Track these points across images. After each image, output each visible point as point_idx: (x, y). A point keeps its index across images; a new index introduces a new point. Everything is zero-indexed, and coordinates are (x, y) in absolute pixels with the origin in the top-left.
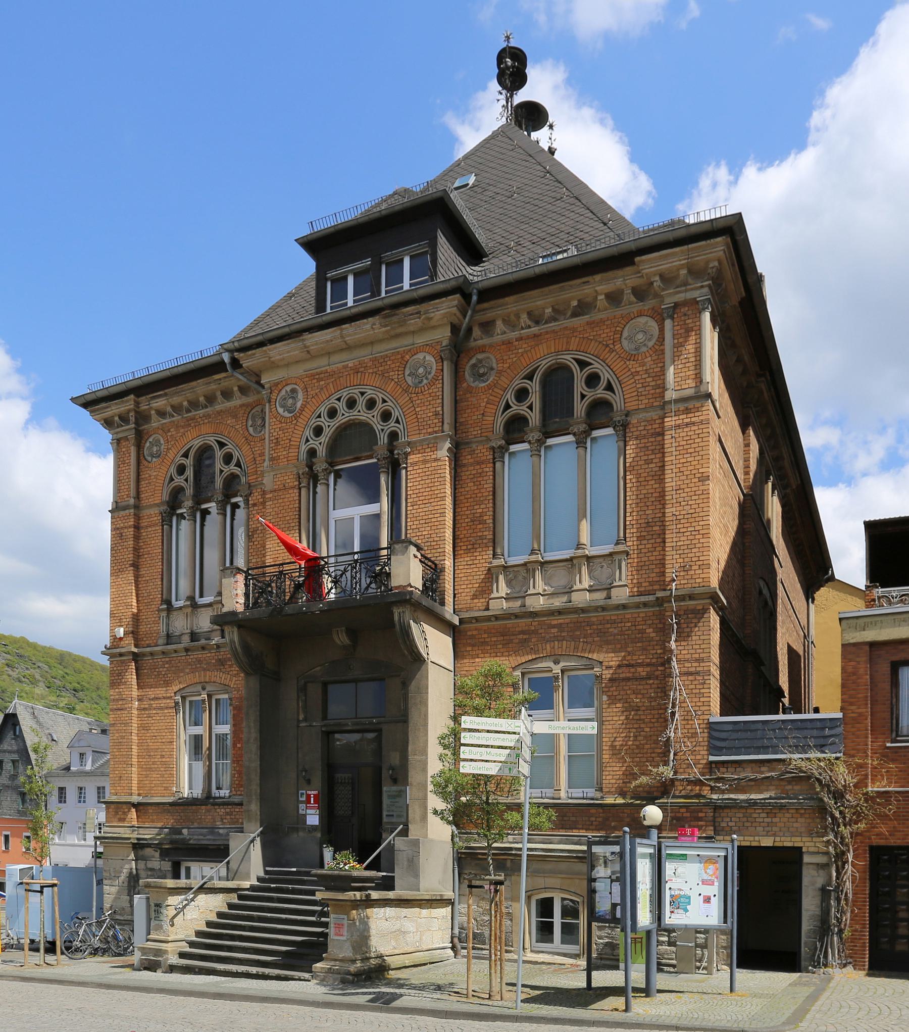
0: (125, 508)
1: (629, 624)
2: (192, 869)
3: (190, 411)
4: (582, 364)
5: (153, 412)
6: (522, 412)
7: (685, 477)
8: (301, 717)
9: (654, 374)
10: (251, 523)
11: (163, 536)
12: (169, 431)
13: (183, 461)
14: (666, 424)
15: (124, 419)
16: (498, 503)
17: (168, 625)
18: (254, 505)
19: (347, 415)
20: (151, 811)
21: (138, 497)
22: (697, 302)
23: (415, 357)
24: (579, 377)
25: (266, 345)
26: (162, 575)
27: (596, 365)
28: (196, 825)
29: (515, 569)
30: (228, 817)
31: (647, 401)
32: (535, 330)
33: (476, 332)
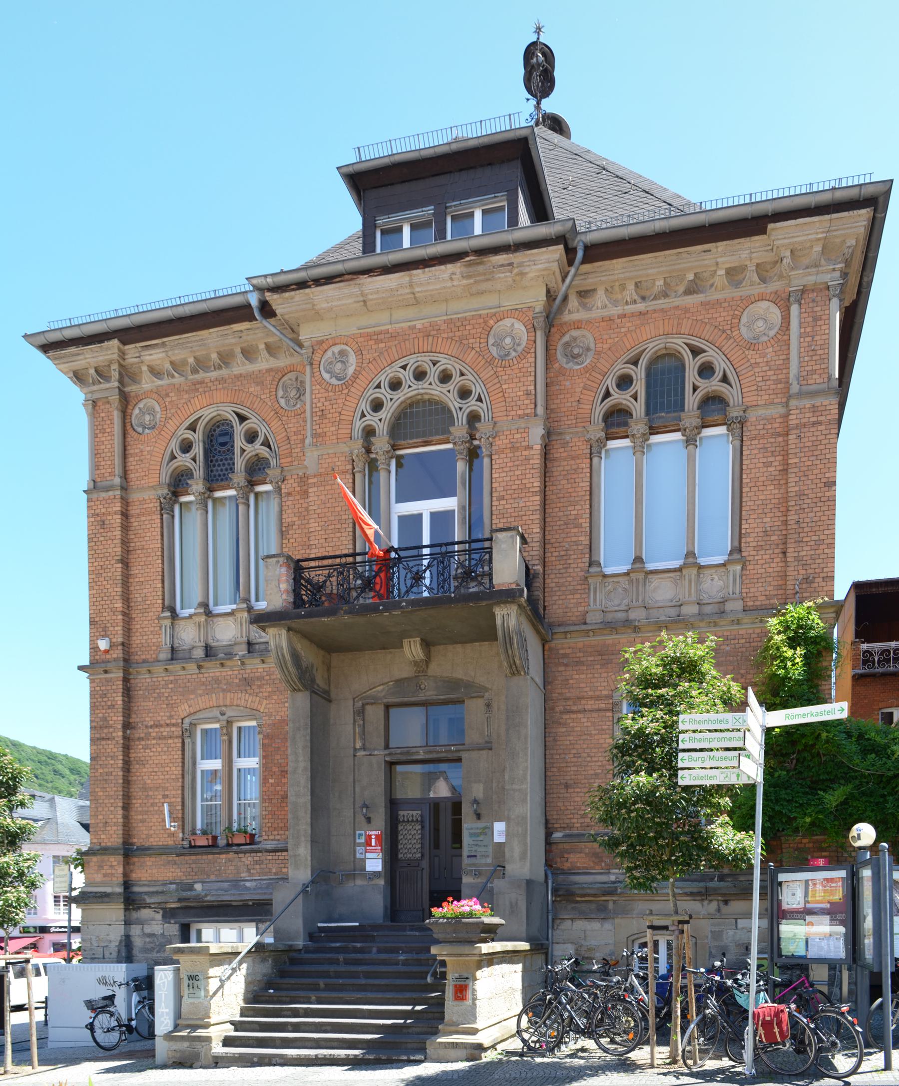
0: (107, 489)
1: (744, 641)
2: (13, 1003)
3: (198, 372)
4: (696, 352)
5: (145, 368)
6: (624, 402)
7: (810, 482)
8: (359, 745)
9: (775, 367)
10: (284, 516)
11: (162, 527)
12: (167, 395)
13: (189, 435)
14: (790, 423)
15: (102, 374)
16: (595, 503)
17: (172, 637)
18: (289, 494)
19: (414, 387)
20: (149, 863)
21: (125, 475)
22: (828, 288)
23: (500, 323)
24: (692, 366)
25: (309, 287)
26: (163, 576)
27: (711, 352)
28: (213, 878)
29: (615, 579)
30: (257, 867)
31: (767, 397)
32: (641, 306)
33: (573, 302)
